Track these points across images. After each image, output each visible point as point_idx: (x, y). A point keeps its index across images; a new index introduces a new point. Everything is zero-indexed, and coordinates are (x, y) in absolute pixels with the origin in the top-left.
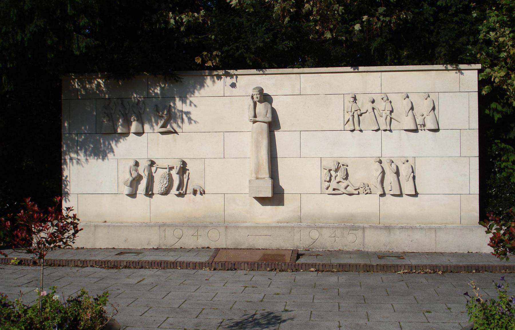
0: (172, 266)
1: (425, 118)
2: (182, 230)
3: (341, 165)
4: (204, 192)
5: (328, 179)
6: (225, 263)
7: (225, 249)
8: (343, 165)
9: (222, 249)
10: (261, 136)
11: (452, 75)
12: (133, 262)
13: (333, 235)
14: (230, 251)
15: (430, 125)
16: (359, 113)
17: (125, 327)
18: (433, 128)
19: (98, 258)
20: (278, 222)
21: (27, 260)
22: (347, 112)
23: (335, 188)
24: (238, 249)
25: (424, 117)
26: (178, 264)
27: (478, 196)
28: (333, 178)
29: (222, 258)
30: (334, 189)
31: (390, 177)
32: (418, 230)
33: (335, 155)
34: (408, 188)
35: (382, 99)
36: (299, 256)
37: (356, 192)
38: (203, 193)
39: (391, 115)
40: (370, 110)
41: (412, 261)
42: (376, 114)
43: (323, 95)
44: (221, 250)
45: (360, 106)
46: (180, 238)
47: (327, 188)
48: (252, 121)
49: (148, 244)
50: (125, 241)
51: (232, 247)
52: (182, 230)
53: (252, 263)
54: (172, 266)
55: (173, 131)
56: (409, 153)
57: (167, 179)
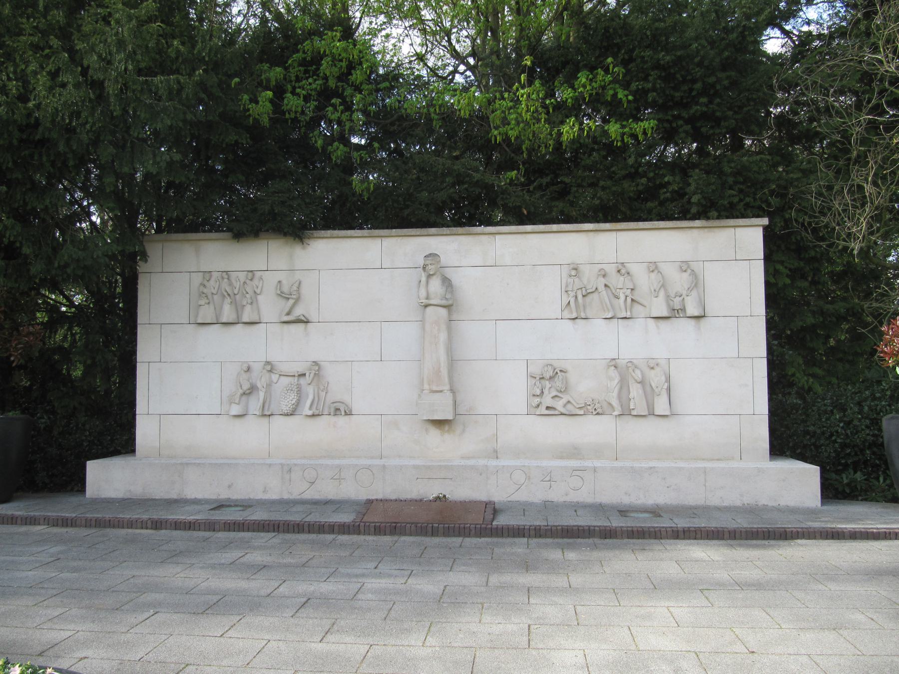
0: (296, 530)
1: (684, 299)
2: (316, 470)
4: (351, 411)
5: (538, 392)
6: (379, 524)
7: (381, 500)
8: (561, 371)
9: (377, 500)
10: (437, 328)
11: (197, 497)
13: (547, 479)
15: (692, 310)
17: (183, 666)
18: (696, 314)
21: (67, 519)
22: (566, 291)
23: (549, 405)
25: (682, 298)
27: (767, 417)
28: (546, 391)
29: (375, 518)
30: (548, 408)
31: (635, 391)
32: (454, 317)
34: (661, 406)
35: (619, 271)
36: (496, 512)
37: (582, 412)
38: (349, 413)
39: (632, 295)
40: (601, 287)
44: (375, 502)
45: (585, 282)
48: (422, 304)
49: (263, 492)
50: (229, 487)
51: (393, 497)
52: (316, 470)
54: (296, 530)
57: (295, 392)
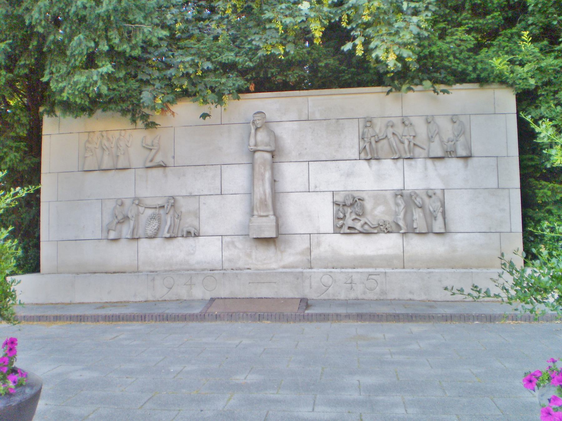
3: (357, 200)
10: (263, 168)
12: (113, 316)
14: (227, 300)
16: (377, 139)
19: (73, 313)
20: (284, 267)
24: (222, 298)
26: (86, 318)
30: (349, 228)
33: (350, 188)
34: (438, 226)
41: (446, 310)
42: (352, 92)
43: (422, 191)
46: (171, 288)
47: (341, 227)
53: (252, 314)
55: (164, 165)
56: (436, 184)
